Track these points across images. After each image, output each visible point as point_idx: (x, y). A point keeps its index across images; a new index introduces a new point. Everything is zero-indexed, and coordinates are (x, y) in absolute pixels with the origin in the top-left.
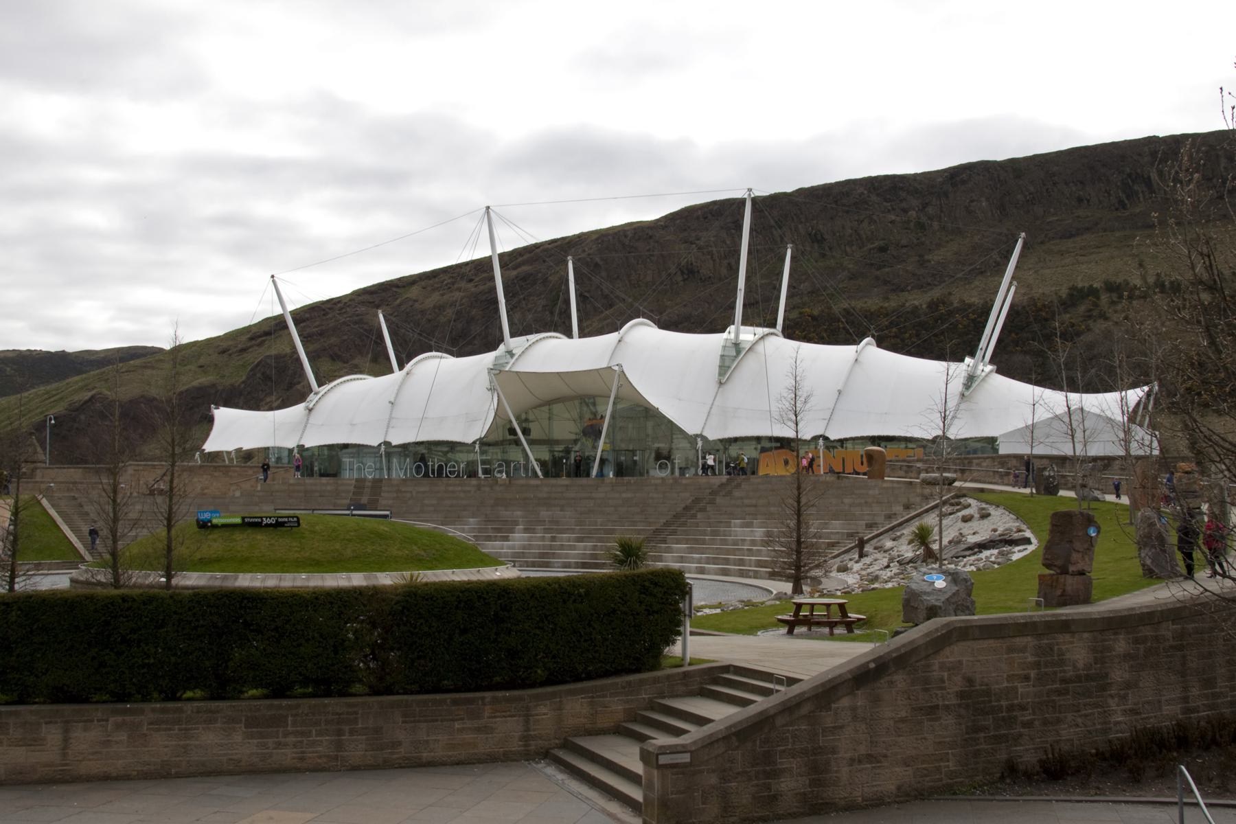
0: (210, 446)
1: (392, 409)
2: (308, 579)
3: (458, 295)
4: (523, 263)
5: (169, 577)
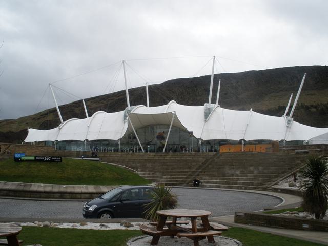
0: (26, 141)
2: (66, 187)
3: (101, 104)
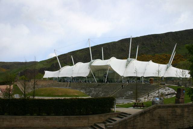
0: (44, 77)
1: (146, 67)
4: (95, 48)
5: (34, 97)
